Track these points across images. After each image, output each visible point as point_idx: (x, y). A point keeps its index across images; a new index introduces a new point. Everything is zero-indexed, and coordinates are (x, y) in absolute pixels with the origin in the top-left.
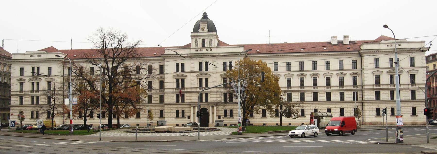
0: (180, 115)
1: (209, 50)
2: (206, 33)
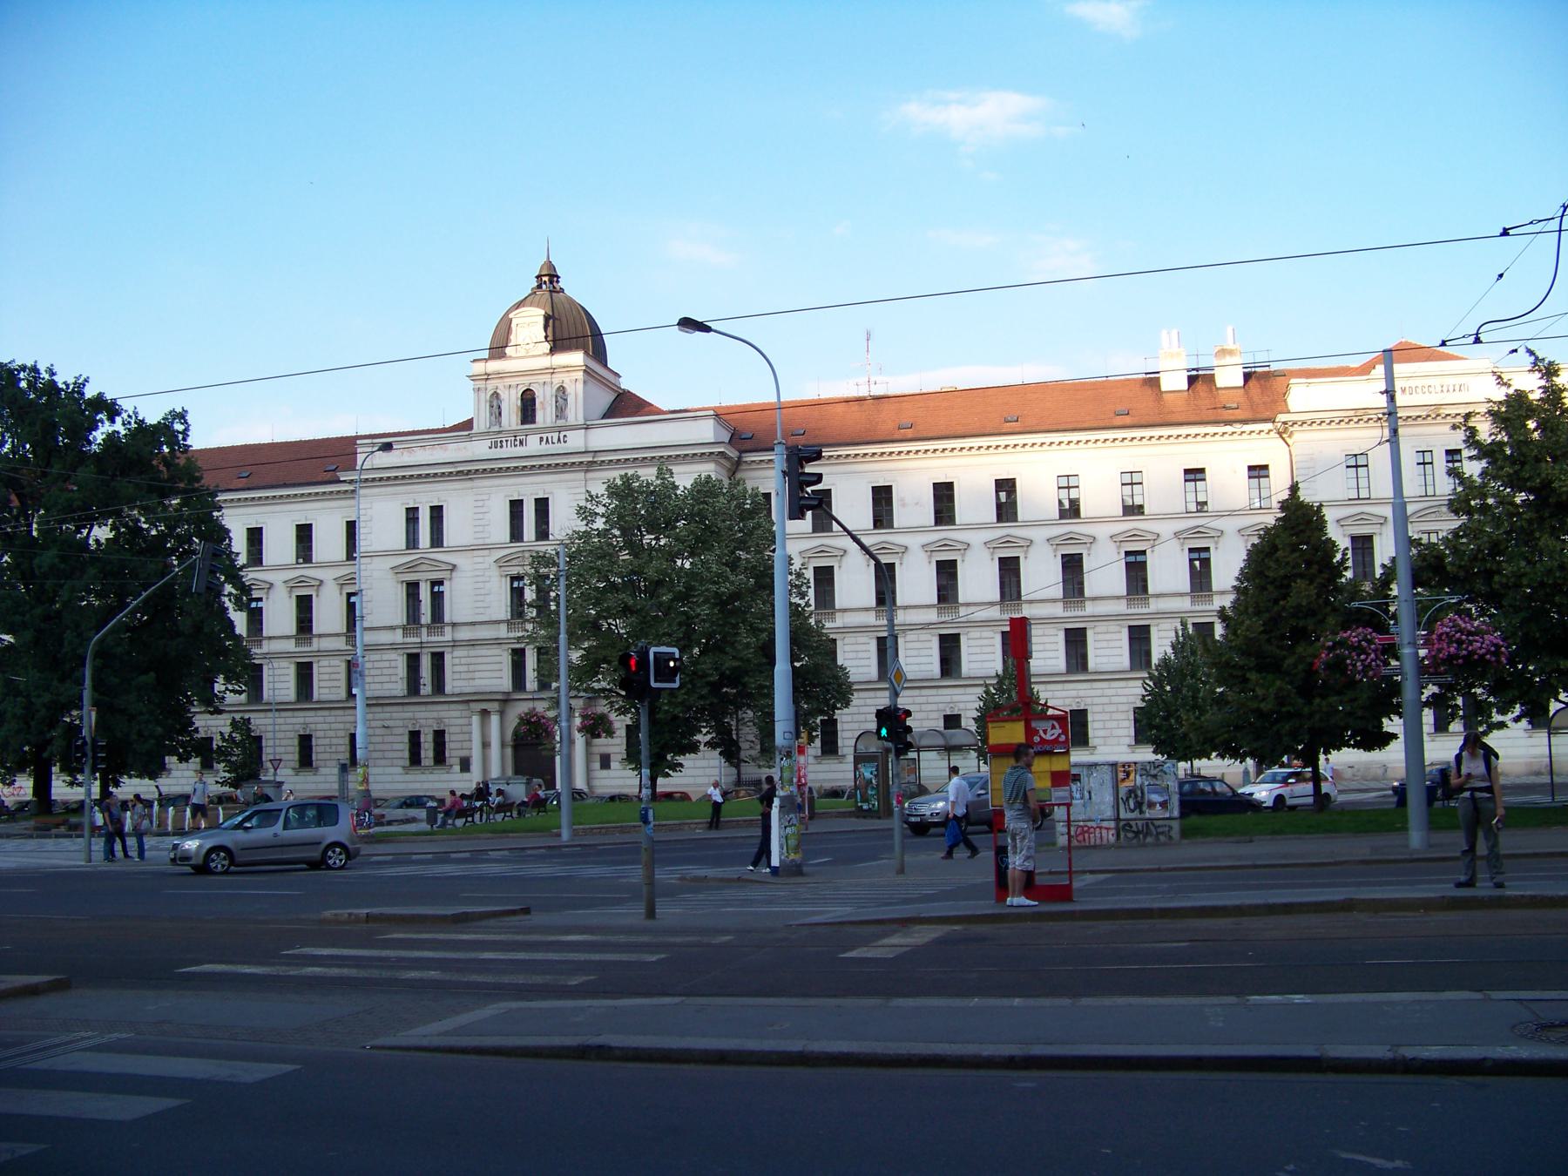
1: (555, 440)
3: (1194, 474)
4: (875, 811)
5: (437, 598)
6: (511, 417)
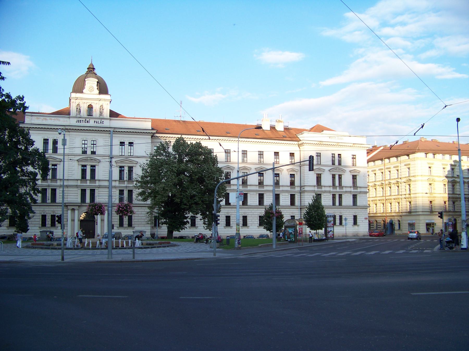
1: (100, 122)
2: (95, 95)
3: (276, 154)
4: (293, 241)
5: (93, 171)
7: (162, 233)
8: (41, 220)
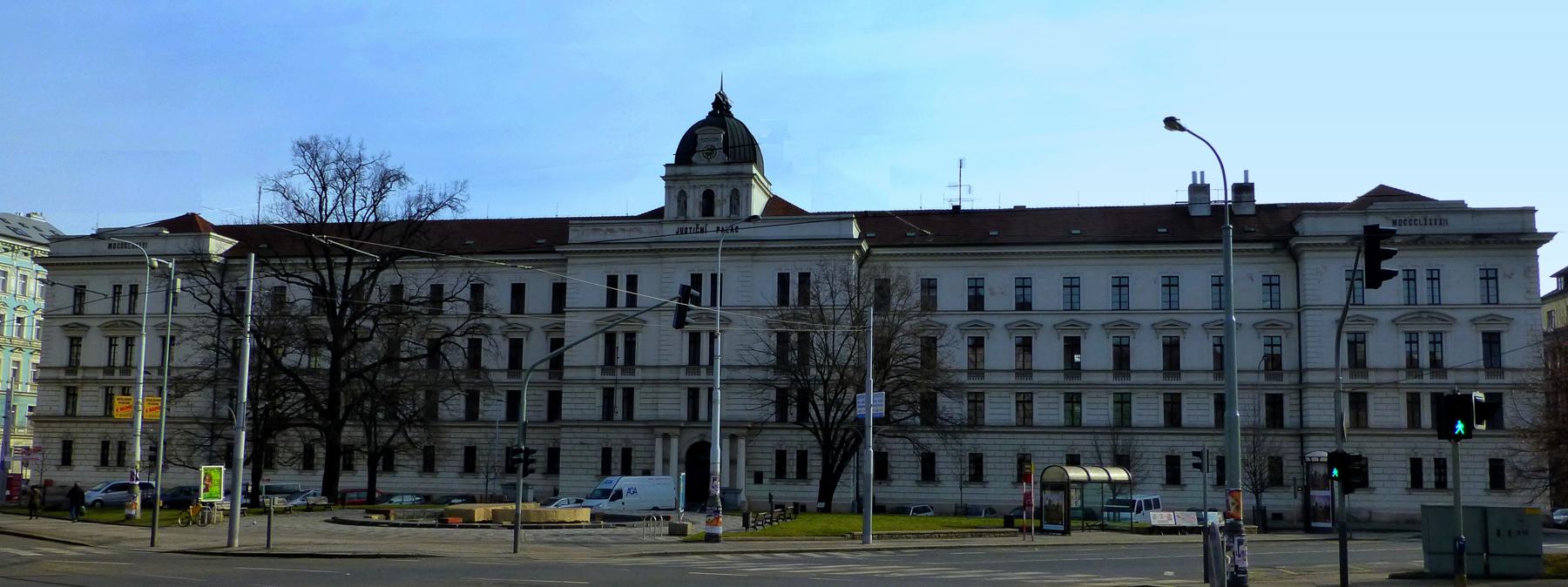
0: (792, 467)
6: (694, 209)
7: (894, 496)
8: (600, 460)
